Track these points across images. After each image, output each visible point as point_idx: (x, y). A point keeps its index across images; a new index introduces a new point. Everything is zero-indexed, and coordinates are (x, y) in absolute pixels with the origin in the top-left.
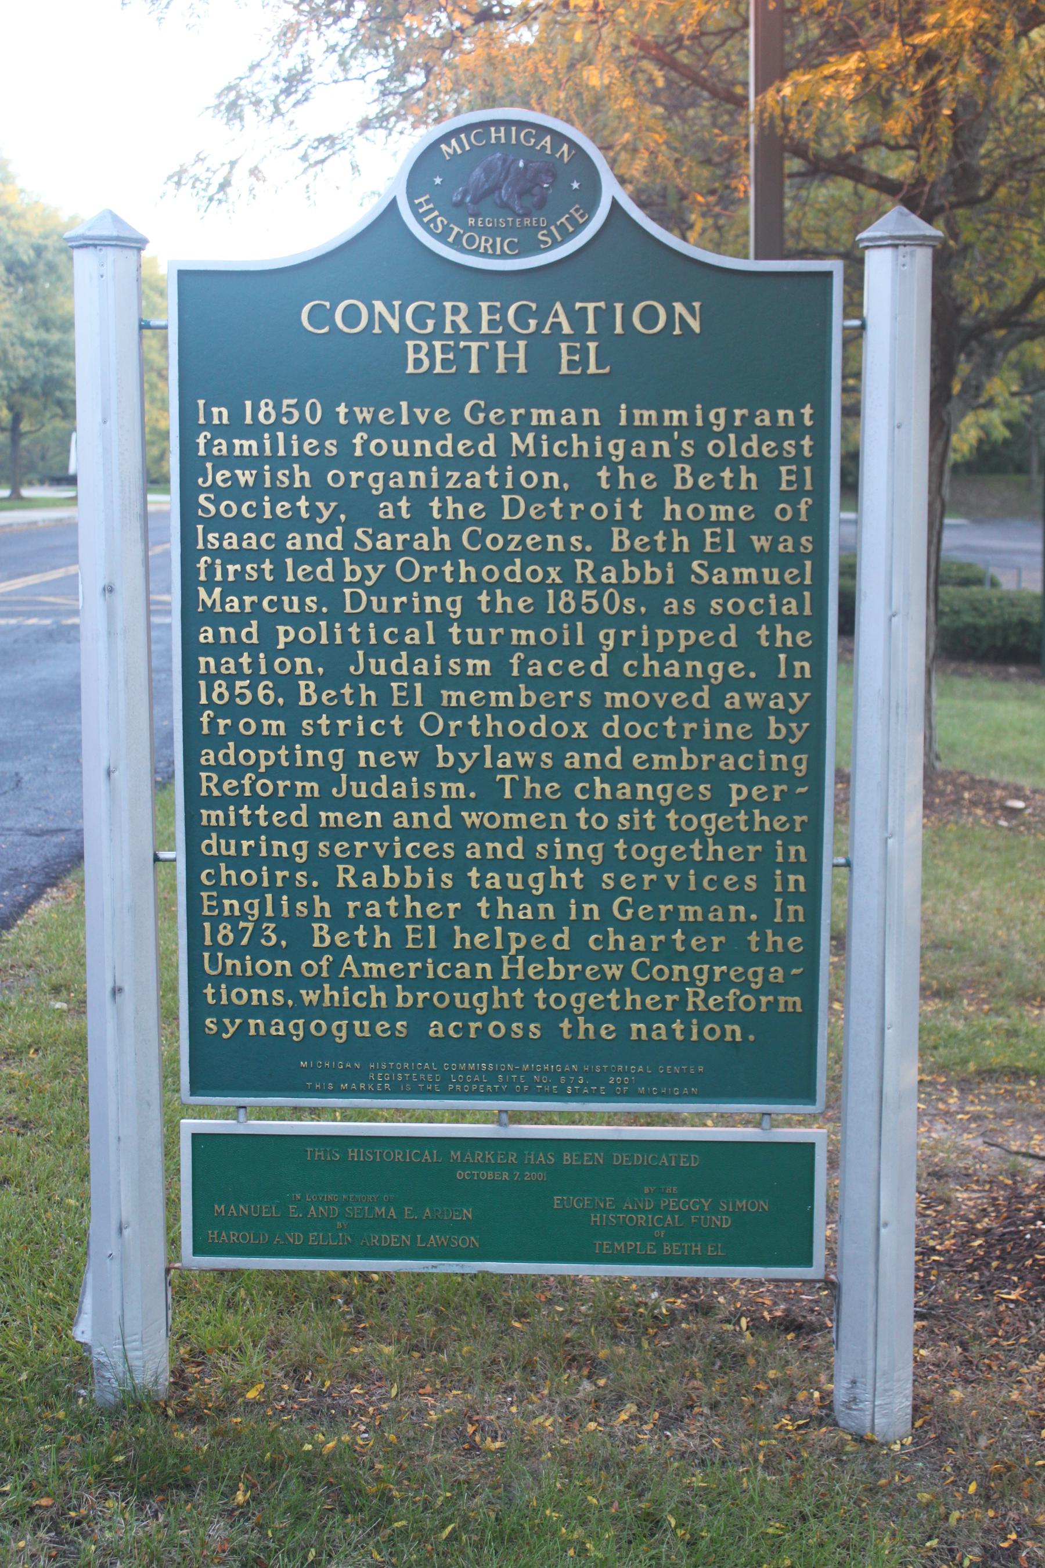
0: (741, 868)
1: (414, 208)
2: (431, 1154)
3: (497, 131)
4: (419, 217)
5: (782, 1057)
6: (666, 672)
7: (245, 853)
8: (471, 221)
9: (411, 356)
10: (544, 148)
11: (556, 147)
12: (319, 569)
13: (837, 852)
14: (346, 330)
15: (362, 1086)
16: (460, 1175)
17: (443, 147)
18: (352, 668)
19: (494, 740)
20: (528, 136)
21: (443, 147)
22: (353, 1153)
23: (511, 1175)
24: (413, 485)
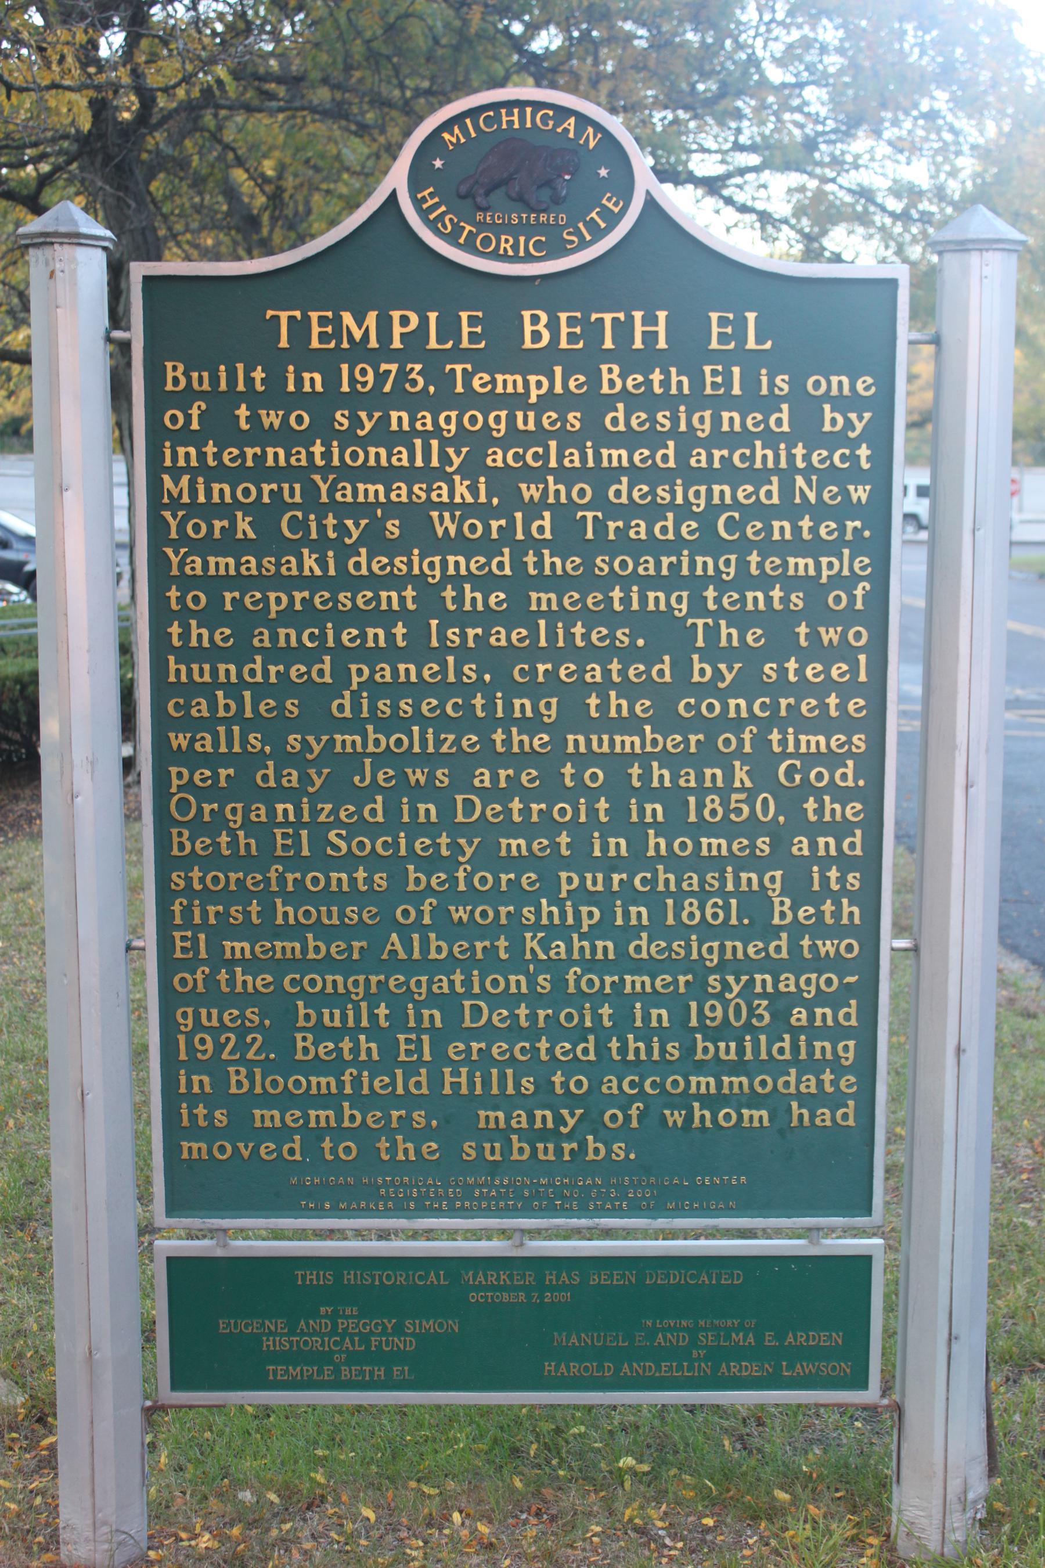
0: (836, 1002)
1: (418, 203)
2: (438, 1276)
3: (510, 114)
4: (423, 214)
5: (836, 1169)
6: (394, 459)
7: (273, 679)
8: (479, 217)
9: (528, 329)
10: (566, 130)
11: (580, 130)
12: (286, 1147)
13: (900, 930)
14: (191, 798)
15: (363, 1204)
16: (474, 1297)
17: (446, 136)
18: (357, 779)
19: (582, 962)
20: (545, 118)
21: (446, 136)
22: (350, 1277)
23: (529, 1296)
24: (744, 887)
